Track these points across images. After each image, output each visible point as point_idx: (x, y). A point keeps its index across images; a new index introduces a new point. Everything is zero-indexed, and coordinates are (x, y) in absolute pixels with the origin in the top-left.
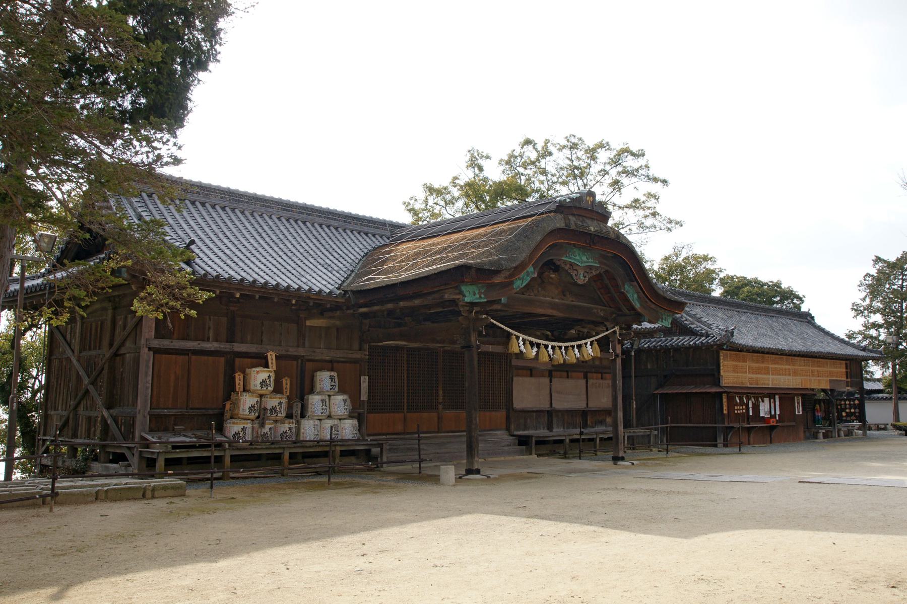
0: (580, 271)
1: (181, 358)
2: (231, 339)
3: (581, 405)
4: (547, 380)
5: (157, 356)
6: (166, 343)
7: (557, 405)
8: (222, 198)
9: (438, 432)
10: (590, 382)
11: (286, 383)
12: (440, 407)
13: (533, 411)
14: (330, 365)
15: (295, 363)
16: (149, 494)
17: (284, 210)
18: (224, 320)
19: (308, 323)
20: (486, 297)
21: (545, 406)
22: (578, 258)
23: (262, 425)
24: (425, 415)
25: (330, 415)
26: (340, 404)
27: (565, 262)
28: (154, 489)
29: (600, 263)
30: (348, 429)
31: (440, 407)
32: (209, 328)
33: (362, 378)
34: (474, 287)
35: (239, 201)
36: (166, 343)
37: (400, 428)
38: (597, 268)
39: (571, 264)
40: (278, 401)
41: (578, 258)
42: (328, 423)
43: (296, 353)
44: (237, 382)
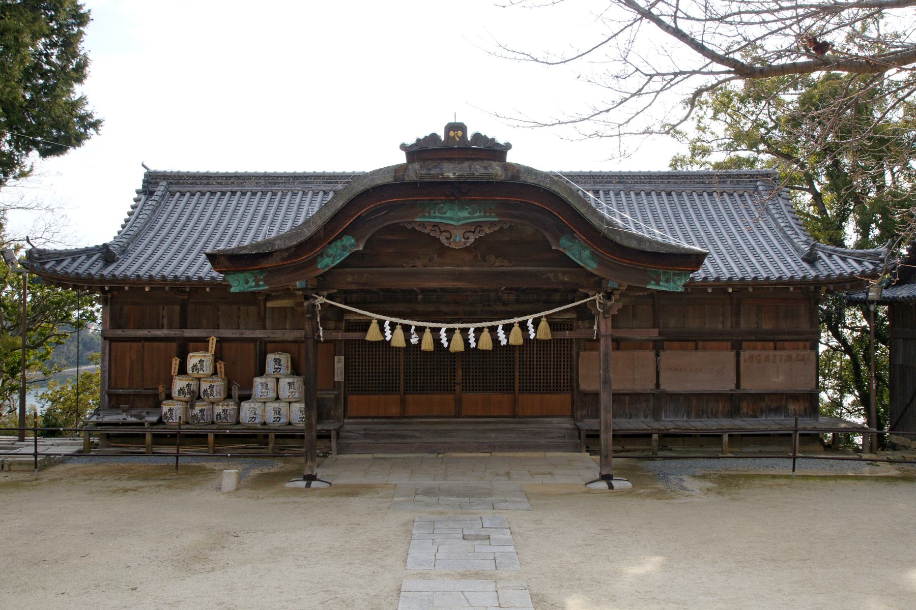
0: (454, 232)
1: (135, 345)
2: (184, 325)
3: (727, 385)
4: (652, 354)
5: (113, 344)
6: (119, 333)
7: (666, 386)
8: (257, 183)
9: (454, 417)
10: (744, 355)
11: (221, 366)
12: (458, 388)
13: (624, 394)
14: (281, 346)
15: (252, 345)
16: (6, 468)
17: (327, 183)
18: (177, 308)
19: (269, 304)
20: (266, 283)
21: (650, 386)
22: (449, 214)
23: (192, 407)
24: (436, 397)
25: (277, 398)
26: (290, 387)
27: (423, 224)
28: (10, 464)
29: (498, 215)
30: (296, 413)
31: (458, 388)
32: (163, 317)
33: (336, 358)
34: (247, 274)
35: (275, 183)
36: (119, 333)
37: (395, 410)
38: (492, 224)
39: (435, 225)
40: (209, 384)
41: (437, 214)
42: (271, 406)
43: (252, 336)
44: (173, 366)
